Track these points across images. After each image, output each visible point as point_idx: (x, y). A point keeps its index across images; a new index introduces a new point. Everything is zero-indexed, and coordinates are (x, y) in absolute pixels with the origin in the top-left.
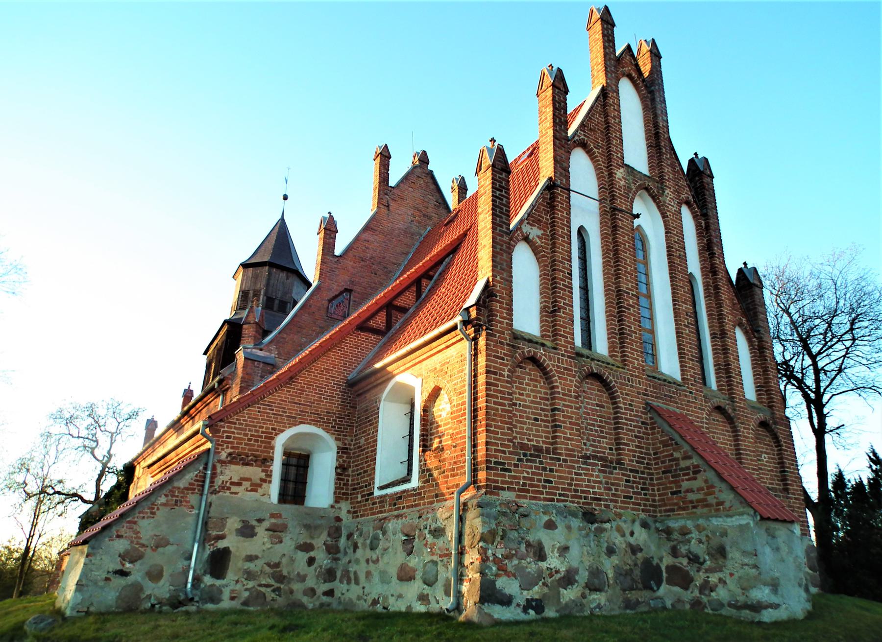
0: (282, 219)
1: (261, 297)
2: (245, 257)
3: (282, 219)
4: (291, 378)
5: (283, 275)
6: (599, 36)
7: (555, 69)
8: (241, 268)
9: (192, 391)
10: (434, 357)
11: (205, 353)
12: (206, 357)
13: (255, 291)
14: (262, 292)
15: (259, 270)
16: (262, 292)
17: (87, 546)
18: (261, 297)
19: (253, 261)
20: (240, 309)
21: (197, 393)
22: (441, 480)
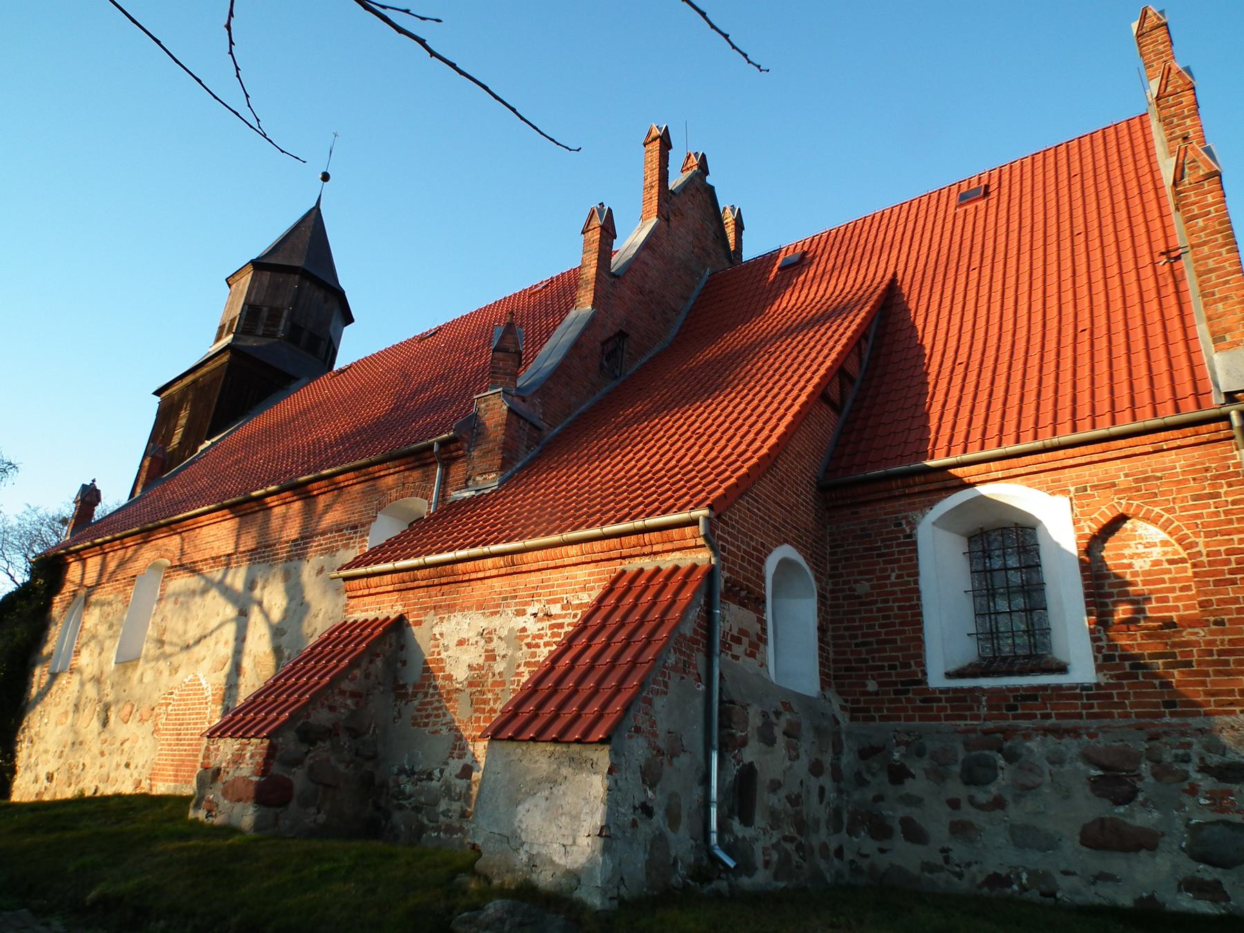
0: (317, 209)
1: (283, 322)
2: (258, 248)
3: (317, 209)
4: (354, 527)
5: (319, 295)
6: (656, 154)
7: (606, 208)
8: (250, 268)
9: (98, 493)
10: (701, 718)
11: (157, 393)
12: (158, 399)
13: (271, 309)
14: (285, 314)
15: (281, 278)
16: (285, 314)
17: (607, 748)
18: (283, 322)
19: (273, 261)
20: (242, 333)
21: (114, 496)
22: (199, 765)
